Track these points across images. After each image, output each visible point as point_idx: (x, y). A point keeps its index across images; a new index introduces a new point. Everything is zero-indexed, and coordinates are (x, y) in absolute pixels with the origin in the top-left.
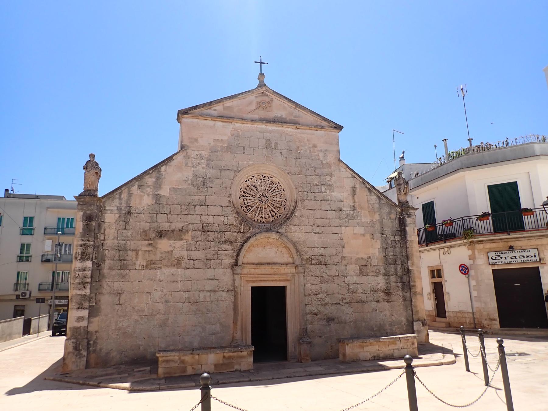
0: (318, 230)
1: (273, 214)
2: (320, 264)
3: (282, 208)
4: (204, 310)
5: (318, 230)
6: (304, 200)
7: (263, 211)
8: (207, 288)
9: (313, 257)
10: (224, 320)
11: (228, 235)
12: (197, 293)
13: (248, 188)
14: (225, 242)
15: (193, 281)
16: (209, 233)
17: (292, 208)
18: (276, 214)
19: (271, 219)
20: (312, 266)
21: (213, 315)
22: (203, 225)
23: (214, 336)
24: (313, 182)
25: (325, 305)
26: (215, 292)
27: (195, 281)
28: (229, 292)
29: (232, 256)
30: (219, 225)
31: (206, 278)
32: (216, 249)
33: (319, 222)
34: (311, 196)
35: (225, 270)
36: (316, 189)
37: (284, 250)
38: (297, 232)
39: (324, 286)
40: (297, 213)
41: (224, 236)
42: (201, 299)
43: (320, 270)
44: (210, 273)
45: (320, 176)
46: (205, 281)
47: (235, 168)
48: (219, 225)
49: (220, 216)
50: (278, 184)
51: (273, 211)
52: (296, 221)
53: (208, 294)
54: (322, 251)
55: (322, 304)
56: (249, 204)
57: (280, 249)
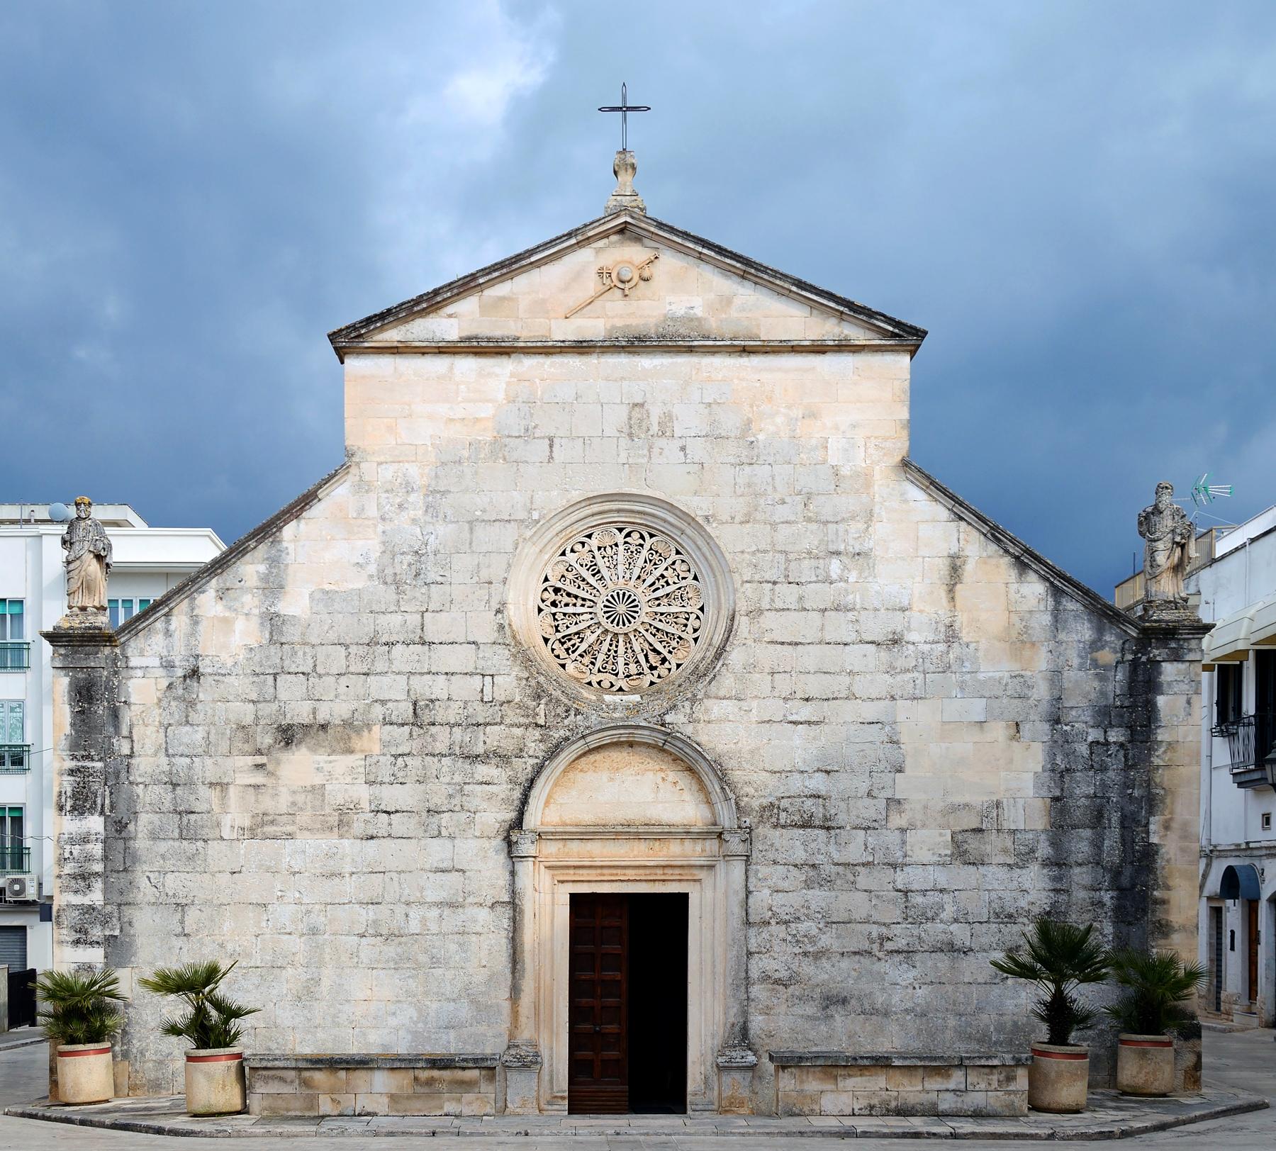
0: (806, 712)
1: (654, 659)
3: (689, 636)
4: (423, 958)
6: (760, 612)
7: (621, 649)
8: (431, 896)
13: (570, 576)
16: (433, 729)
17: (717, 641)
18: (664, 660)
19: (648, 678)
20: (779, 831)
21: (450, 974)
22: (415, 704)
23: (452, 1034)
25: (818, 956)
26: (451, 905)
27: (394, 875)
30: (466, 702)
31: (427, 867)
32: (458, 778)
33: (814, 686)
34: (788, 594)
35: (485, 843)
36: (805, 570)
37: (684, 780)
39: (818, 897)
40: (735, 656)
41: (482, 738)
42: (414, 926)
44: (438, 852)
47: (522, 515)
48: (466, 702)
49: (472, 674)
51: (655, 650)
52: (727, 682)
53: (435, 912)
54: (818, 783)
56: (573, 629)
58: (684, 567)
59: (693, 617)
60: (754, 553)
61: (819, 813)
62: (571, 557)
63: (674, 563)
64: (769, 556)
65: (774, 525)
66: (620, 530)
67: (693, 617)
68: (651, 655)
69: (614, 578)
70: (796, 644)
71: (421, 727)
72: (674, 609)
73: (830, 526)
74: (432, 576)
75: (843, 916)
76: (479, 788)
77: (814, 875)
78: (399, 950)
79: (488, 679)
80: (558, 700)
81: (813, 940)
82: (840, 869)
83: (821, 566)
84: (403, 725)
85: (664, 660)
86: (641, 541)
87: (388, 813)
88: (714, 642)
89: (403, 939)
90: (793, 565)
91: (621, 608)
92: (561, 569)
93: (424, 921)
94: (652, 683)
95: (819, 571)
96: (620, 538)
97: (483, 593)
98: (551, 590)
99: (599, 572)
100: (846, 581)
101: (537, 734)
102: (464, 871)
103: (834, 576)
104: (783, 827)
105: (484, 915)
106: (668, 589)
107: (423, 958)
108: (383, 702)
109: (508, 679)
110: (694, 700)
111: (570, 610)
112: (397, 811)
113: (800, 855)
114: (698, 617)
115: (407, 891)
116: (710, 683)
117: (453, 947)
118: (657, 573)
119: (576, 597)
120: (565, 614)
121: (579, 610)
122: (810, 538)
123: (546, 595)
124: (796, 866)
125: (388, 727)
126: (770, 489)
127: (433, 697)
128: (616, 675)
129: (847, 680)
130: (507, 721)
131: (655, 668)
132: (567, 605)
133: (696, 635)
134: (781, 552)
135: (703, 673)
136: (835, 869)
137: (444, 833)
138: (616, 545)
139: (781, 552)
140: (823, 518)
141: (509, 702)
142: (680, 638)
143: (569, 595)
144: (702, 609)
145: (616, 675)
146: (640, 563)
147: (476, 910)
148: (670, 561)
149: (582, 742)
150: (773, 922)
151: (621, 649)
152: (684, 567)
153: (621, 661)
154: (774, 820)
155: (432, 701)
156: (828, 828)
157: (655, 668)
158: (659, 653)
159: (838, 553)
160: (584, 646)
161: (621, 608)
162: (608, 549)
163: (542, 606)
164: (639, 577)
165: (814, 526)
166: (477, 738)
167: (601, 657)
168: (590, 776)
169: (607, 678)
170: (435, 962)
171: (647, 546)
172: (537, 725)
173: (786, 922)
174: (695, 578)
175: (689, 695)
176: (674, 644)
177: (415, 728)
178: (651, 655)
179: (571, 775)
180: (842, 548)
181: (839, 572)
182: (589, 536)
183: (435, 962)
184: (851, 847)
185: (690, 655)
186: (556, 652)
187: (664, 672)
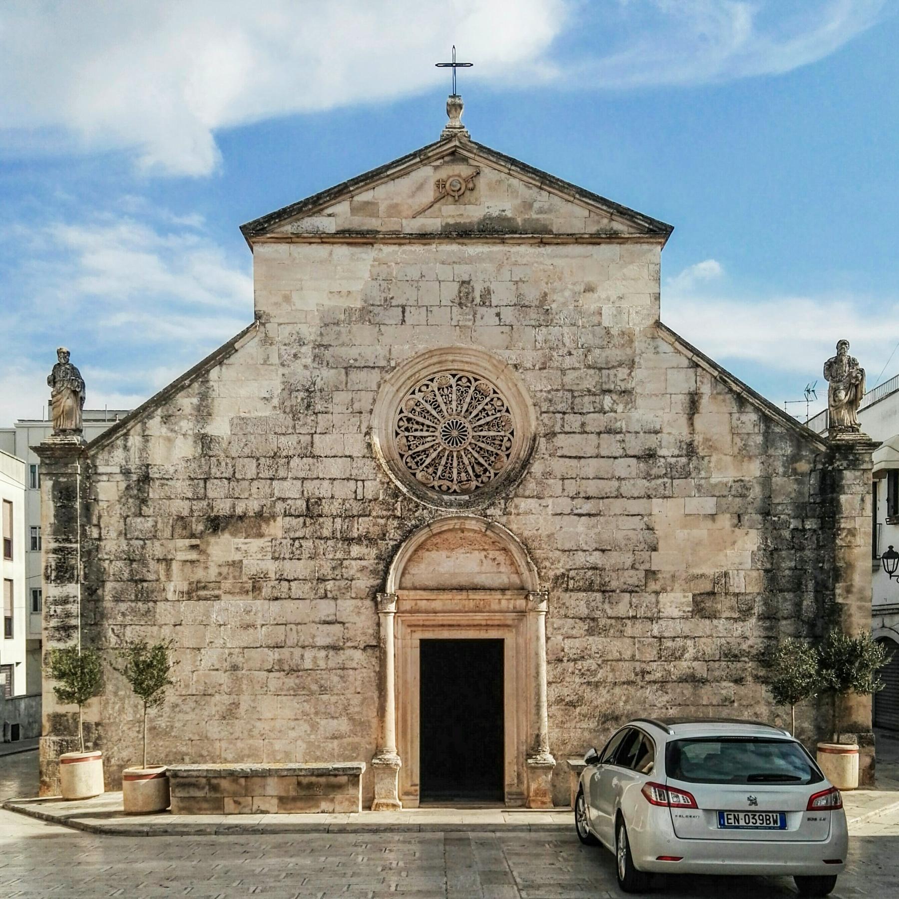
0: (587, 507)
2: (589, 588)
4: (314, 687)
5: (587, 507)
6: (554, 434)
7: (455, 464)
10: (357, 709)
11: (361, 527)
12: (298, 652)
13: (418, 409)
14: (359, 540)
15: (289, 626)
17: (523, 455)
18: (486, 470)
19: (474, 484)
21: (334, 699)
22: (308, 501)
23: (336, 742)
24: (580, 387)
25: (597, 685)
27: (293, 626)
28: (369, 651)
29: (374, 572)
30: (344, 500)
31: (317, 620)
32: (339, 555)
33: (592, 488)
34: (574, 421)
35: (359, 603)
37: (501, 557)
38: (532, 516)
39: (596, 643)
40: (537, 468)
41: (356, 526)
42: (308, 664)
43: (588, 603)
44: (326, 609)
45: (600, 369)
46: (316, 626)
47: (383, 363)
48: (344, 500)
49: (348, 479)
51: (479, 464)
52: (531, 486)
53: (323, 653)
54: (596, 558)
55: (589, 683)
56: (421, 448)
57: (492, 554)
58: (499, 403)
59: (506, 439)
60: (549, 392)
61: (598, 580)
63: (492, 400)
64: (560, 394)
65: (563, 372)
66: (454, 376)
67: (506, 439)
69: (449, 410)
70: (580, 458)
71: (311, 518)
72: (492, 433)
73: (604, 371)
74: (318, 408)
75: (616, 655)
76: (353, 562)
77: (593, 624)
78: (297, 681)
81: (594, 673)
82: (613, 621)
83: (597, 401)
84: (299, 516)
85: (486, 470)
86: (468, 384)
87: (289, 581)
88: (521, 456)
89: (300, 673)
91: (455, 433)
92: (412, 403)
94: (477, 487)
95: (595, 405)
96: (453, 381)
97: (355, 420)
98: (404, 419)
99: (439, 406)
100: (616, 412)
101: (396, 523)
102: (343, 623)
103: (607, 408)
104: (572, 591)
105: (358, 655)
106: (488, 419)
107: (314, 687)
108: (284, 500)
109: (375, 483)
110: (507, 499)
111: (418, 434)
112: (295, 580)
113: (584, 611)
114: (509, 440)
115: (302, 638)
116: (518, 486)
117: (336, 679)
118: (480, 407)
119: (423, 424)
120: (415, 437)
121: (425, 434)
122: (590, 381)
123: (401, 423)
124: (581, 619)
125: (288, 518)
127: (321, 496)
128: (452, 481)
130: (374, 514)
131: (480, 476)
132: (416, 430)
133: (508, 452)
134: (568, 390)
135: (514, 479)
136: (609, 621)
137: (329, 595)
138: (451, 386)
139: (568, 390)
140: (599, 366)
141: (375, 500)
142: (497, 454)
143: (418, 423)
144: (512, 433)
145: (452, 481)
146: (468, 400)
148: (488, 399)
149: (427, 529)
150: (565, 659)
151: (455, 464)
152: (499, 403)
153: (455, 471)
154: (565, 585)
155: (320, 499)
156: (604, 592)
157: (480, 476)
158: (482, 465)
159: (610, 391)
160: (428, 461)
161: (455, 433)
162: (445, 390)
163: (399, 431)
164: (467, 410)
165: (592, 371)
166: (353, 526)
167: (441, 468)
168: (434, 554)
171: (472, 389)
172: (395, 517)
173: (575, 660)
174: (507, 411)
175: (504, 495)
176: (492, 459)
177: (308, 519)
179: (420, 553)
180: (612, 387)
181: (610, 405)
182: (432, 380)
183: (323, 690)
184: (621, 606)
185: (507, 464)
186: (409, 465)
187: (485, 479)
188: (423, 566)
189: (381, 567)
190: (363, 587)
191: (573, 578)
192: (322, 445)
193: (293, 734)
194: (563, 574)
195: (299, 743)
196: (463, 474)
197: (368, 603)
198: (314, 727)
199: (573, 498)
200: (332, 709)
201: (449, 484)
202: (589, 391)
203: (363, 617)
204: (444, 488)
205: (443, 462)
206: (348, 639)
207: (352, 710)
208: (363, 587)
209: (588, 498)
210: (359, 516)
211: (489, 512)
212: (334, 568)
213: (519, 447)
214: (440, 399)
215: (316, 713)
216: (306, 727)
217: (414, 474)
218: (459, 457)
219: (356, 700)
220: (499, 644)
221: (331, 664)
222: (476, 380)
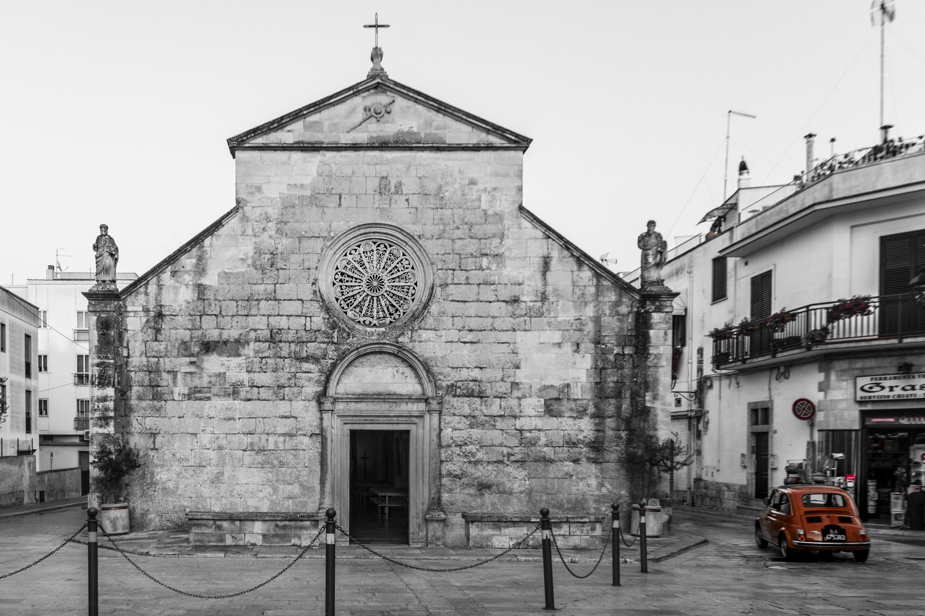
0: (470, 337)
1: (392, 310)
2: (470, 395)
3: (409, 298)
4: (276, 462)
5: (470, 337)
6: (447, 285)
8: (280, 430)
9: (459, 384)
10: (306, 478)
12: (264, 437)
13: (349, 266)
14: (306, 359)
16: (281, 345)
17: (424, 299)
18: (397, 310)
19: (388, 320)
20: (456, 399)
21: (289, 471)
22: (271, 331)
23: (290, 501)
29: (318, 382)
32: (293, 370)
33: (474, 323)
34: (461, 276)
35: (307, 403)
37: (408, 372)
39: (476, 433)
40: (434, 308)
42: (271, 446)
43: (470, 405)
44: (283, 407)
45: (480, 239)
46: (277, 420)
47: (325, 234)
49: (300, 316)
50: (402, 257)
51: (392, 305)
52: (430, 321)
53: (281, 439)
55: (470, 462)
56: (351, 294)
62: (349, 257)
64: (451, 256)
66: (375, 243)
68: (390, 308)
72: (401, 284)
75: (489, 443)
79: (308, 319)
80: (344, 330)
85: (397, 310)
87: (258, 387)
90: (463, 261)
91: (375, 283)
92: (345, 263)
93: (276, 443)
94: (391, 322)
97: (306, 274)
101: (333, 347)
103: (484, 267)
104: (458, 396)
105: (306, 440)
106: (399, 274)
110: (412, 330)
111: (349, 284)
113: (467, 411)
117: (291, 457)
118: (393, 265)
123: (337, 276)
126: (451, 222)
129: (491, 320)
137: (286, 398)
143: (348, 276)
144: (416, 284)
146: (385, 260)
147: (302, 438)
153: (375, 310)
159: (487, 255)
160: (356, 303)
161: (375, 283)
165: (474, 241)
167: (365, 308)
169: (368, 319)
170: (282, 464)
171: (388, 252)
172: (333, 343)
174: (413, 268)
176: (402, 302)
178: (390, 308)
179: (350, 369)
180: (488, 252)
183: (282, 464)
184: (493, 407)
185: (413, 306)
187: (397, 317)
188: (352, 378)
189: (323, 378)
190: (310, 392)
191: (459, 388)
192: (282, 291)
193: (261, 495)
194: (453, 385)
195: (265, 501)
196: (381, 313)
197: (314, 404)
198: (275, 490)
199: (460, 330)
200: (288, 478)
201: (371, 319)
202: (472, 254)
203: (310, 414)
204: (367, 322)
205: (367, 303)
206: (300, 429)
207: (301, 479)
208: (310, 392)
209: (470, 331)
210: (307, 342)
211: (400, 340)
212: (289, 379)
213: (421, 294)
214: (365, 260)
215: (277, 481)
216: (270, 490)
217: (346, 313)
218: (378, 300)
219: (305, 472)
220: (407, 432)
221: (288, 446)
222: (390, 246)
